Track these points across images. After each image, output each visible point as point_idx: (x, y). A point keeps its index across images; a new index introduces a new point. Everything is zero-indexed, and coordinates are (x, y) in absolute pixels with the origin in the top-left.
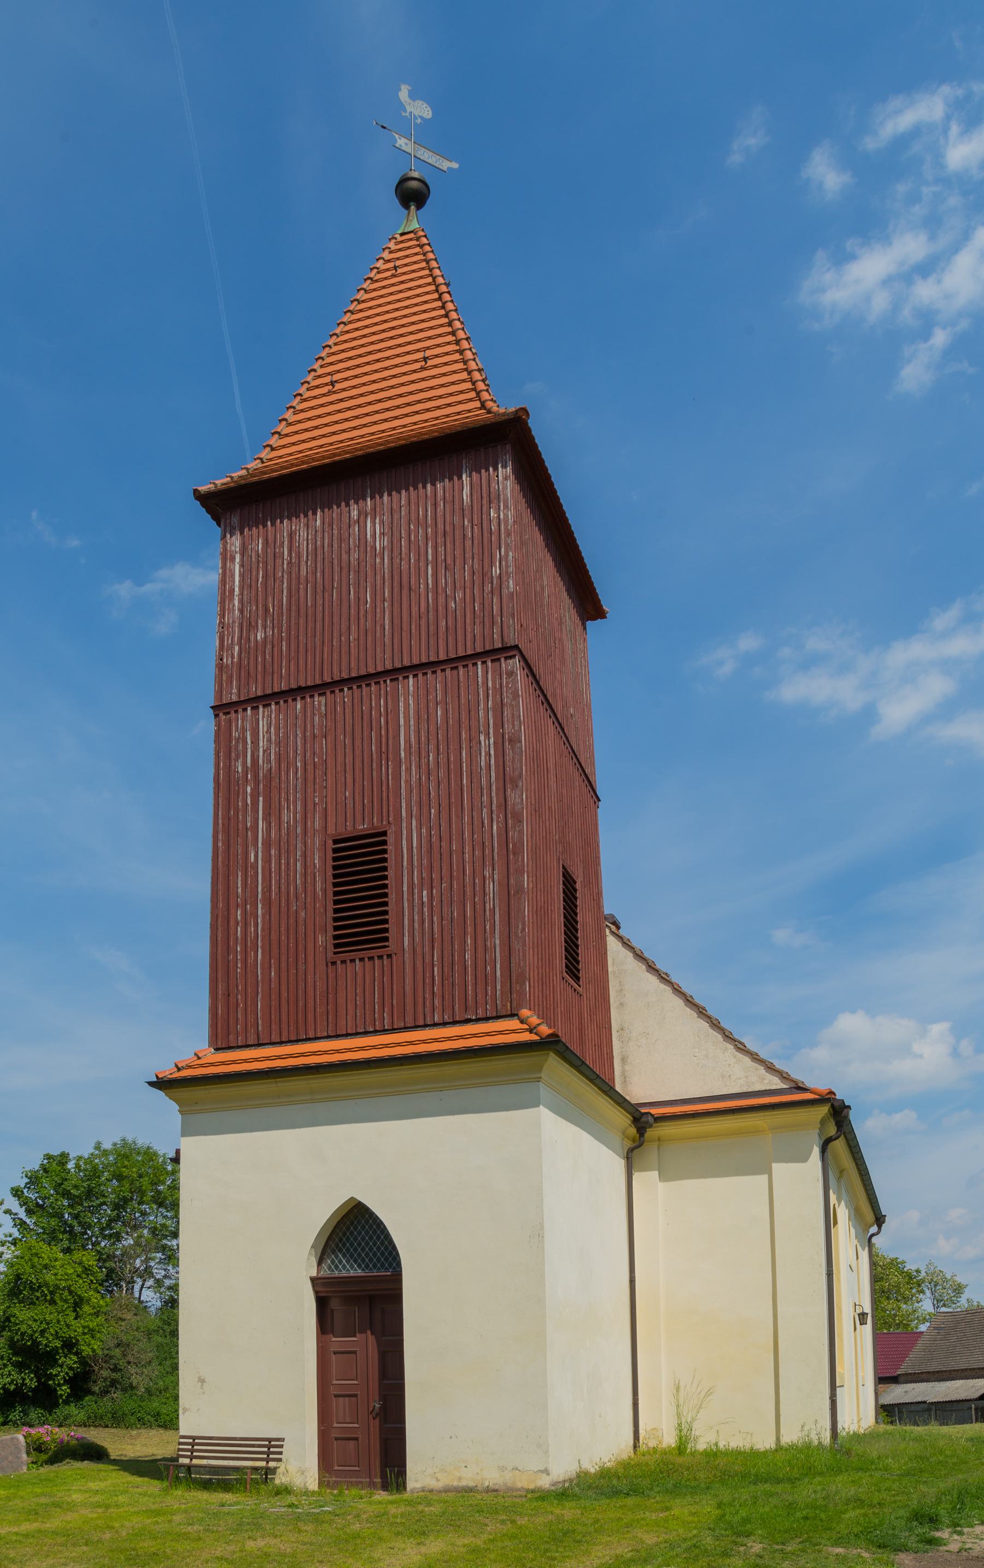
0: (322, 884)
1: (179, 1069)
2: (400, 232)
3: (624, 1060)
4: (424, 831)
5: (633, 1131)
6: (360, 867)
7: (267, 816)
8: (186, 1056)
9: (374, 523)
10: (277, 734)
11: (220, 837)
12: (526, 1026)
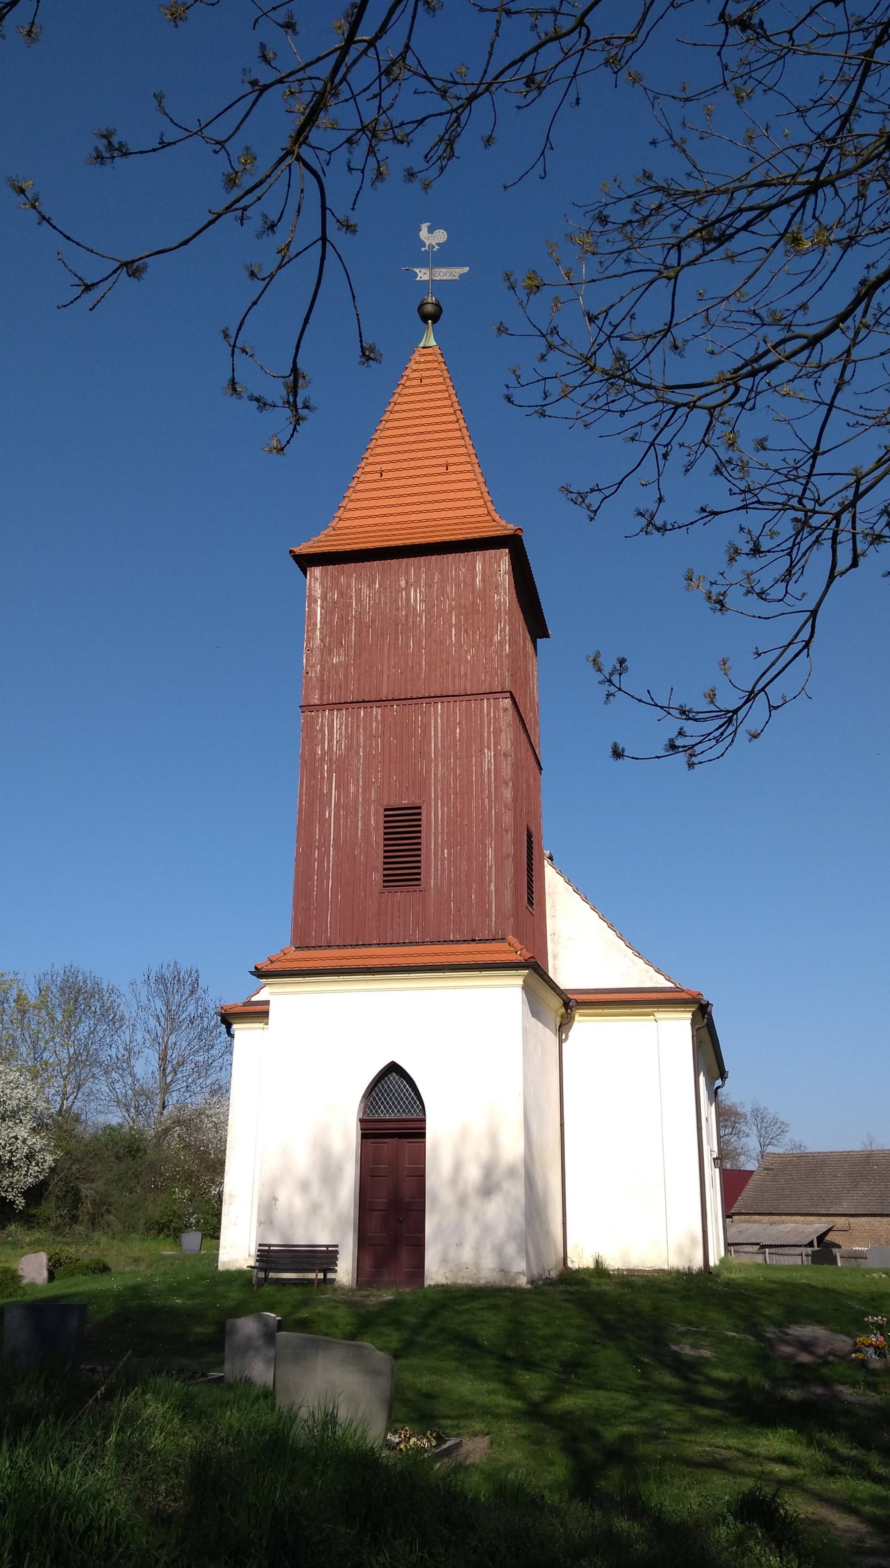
0: (377, 838)
1: (272, 962)
2: (421, 345)
3: (555, 956)
4: (446, 809)
5: (563, 1010)
6: (403, 831)
7: (338, 787)
8: (275, 952)
9: (415, 592)
10: (346, 731)
11: (304, 798)
12: (512, 949)
